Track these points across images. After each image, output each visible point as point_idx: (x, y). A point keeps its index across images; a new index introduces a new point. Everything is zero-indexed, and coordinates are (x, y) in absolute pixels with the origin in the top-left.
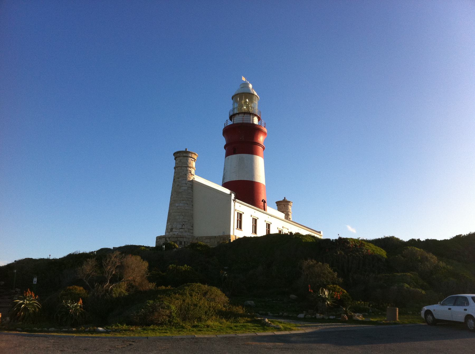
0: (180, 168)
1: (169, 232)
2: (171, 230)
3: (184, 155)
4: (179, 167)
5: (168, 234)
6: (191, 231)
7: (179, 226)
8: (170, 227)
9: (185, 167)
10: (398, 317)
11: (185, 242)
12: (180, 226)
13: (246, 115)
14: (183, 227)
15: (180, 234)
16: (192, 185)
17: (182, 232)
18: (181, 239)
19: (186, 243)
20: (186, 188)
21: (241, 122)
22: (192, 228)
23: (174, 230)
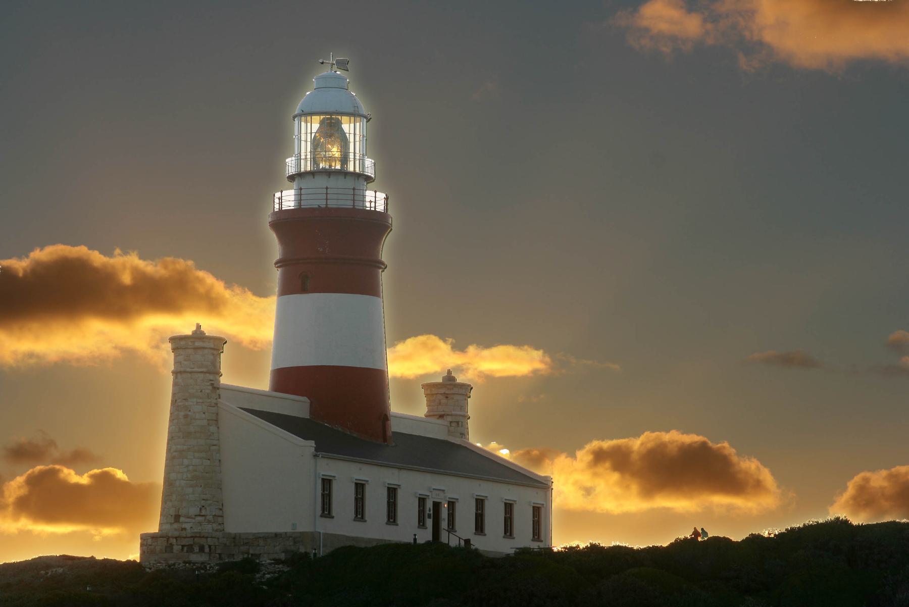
0: (189, 375)
1: (171, 524)
2: (177, 518)
3: (197, 344)
4: (185, 372)
5: (168, 527)
6: (220, 519)
7: (194, 511)
8: (172, 512)
9: (177, 348)
10: (358, 99)
11: (210, 546)
12: (197, 511)
13: (332, 178)
14: (203, 513)
15: (197, 530)
16: (181, 372)
17: (200, 523)
18: (202, 541)
19: (213, 547)
20: (205, 422)
21: (322, 204)
22: (220, 513)
23: (182, 519)
